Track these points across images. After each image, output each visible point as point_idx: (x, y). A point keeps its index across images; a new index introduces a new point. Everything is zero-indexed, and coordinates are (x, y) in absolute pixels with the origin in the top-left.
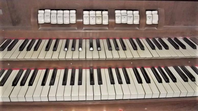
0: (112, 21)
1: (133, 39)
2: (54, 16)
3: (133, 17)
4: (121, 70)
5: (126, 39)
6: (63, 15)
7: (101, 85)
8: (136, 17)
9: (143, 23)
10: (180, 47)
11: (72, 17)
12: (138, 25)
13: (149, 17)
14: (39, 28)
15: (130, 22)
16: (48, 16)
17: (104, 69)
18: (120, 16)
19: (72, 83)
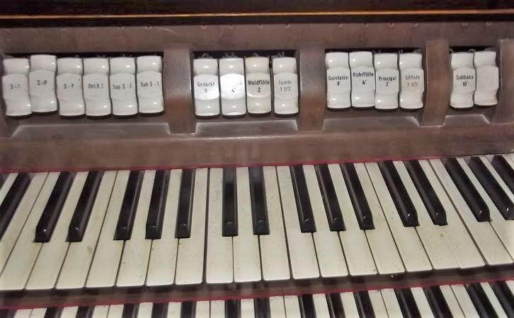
1: (395, 163)
2: (69, 84)
3: (397, 82)
4: (335, 171)
6: (107, 77)
7: (261, 236)
8: (411, 81)
11: (146, 85)
13: (462, 77)
14: (12, 132)
16: (45, 82)
17: (281, 298)
18: (345, 78)
19: (153, 232)
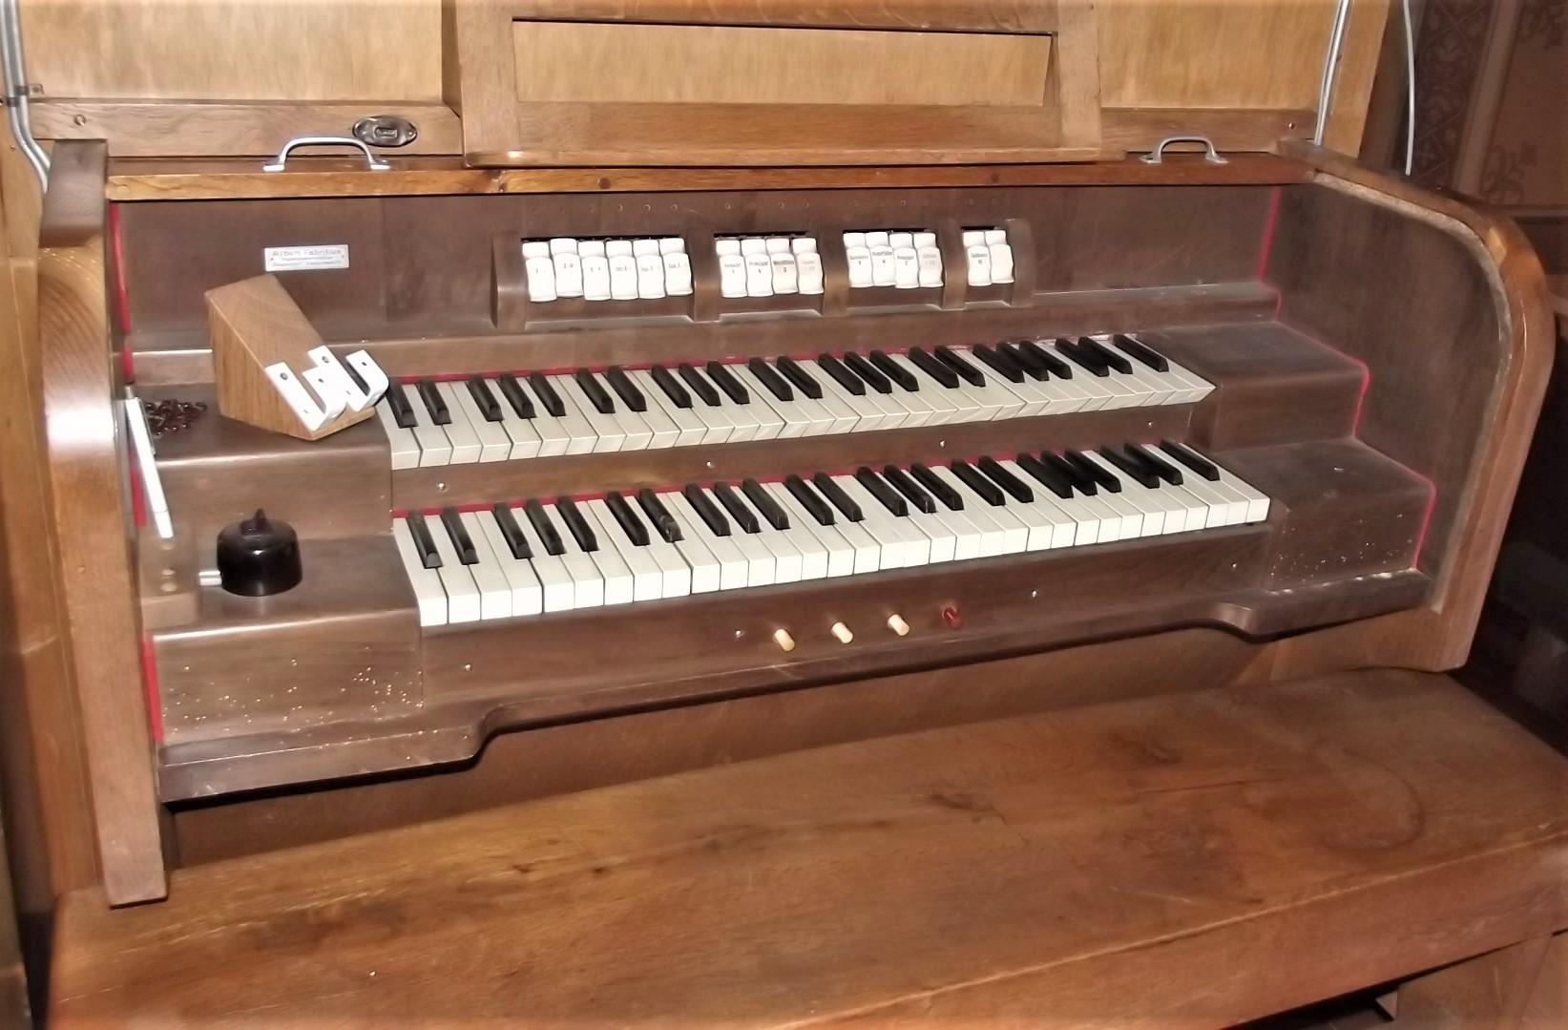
0: (836, 281)
5: (637, 373)
9: (704, 299)
10: (893, 383)
12: (687, 303)
15: (905, 281)
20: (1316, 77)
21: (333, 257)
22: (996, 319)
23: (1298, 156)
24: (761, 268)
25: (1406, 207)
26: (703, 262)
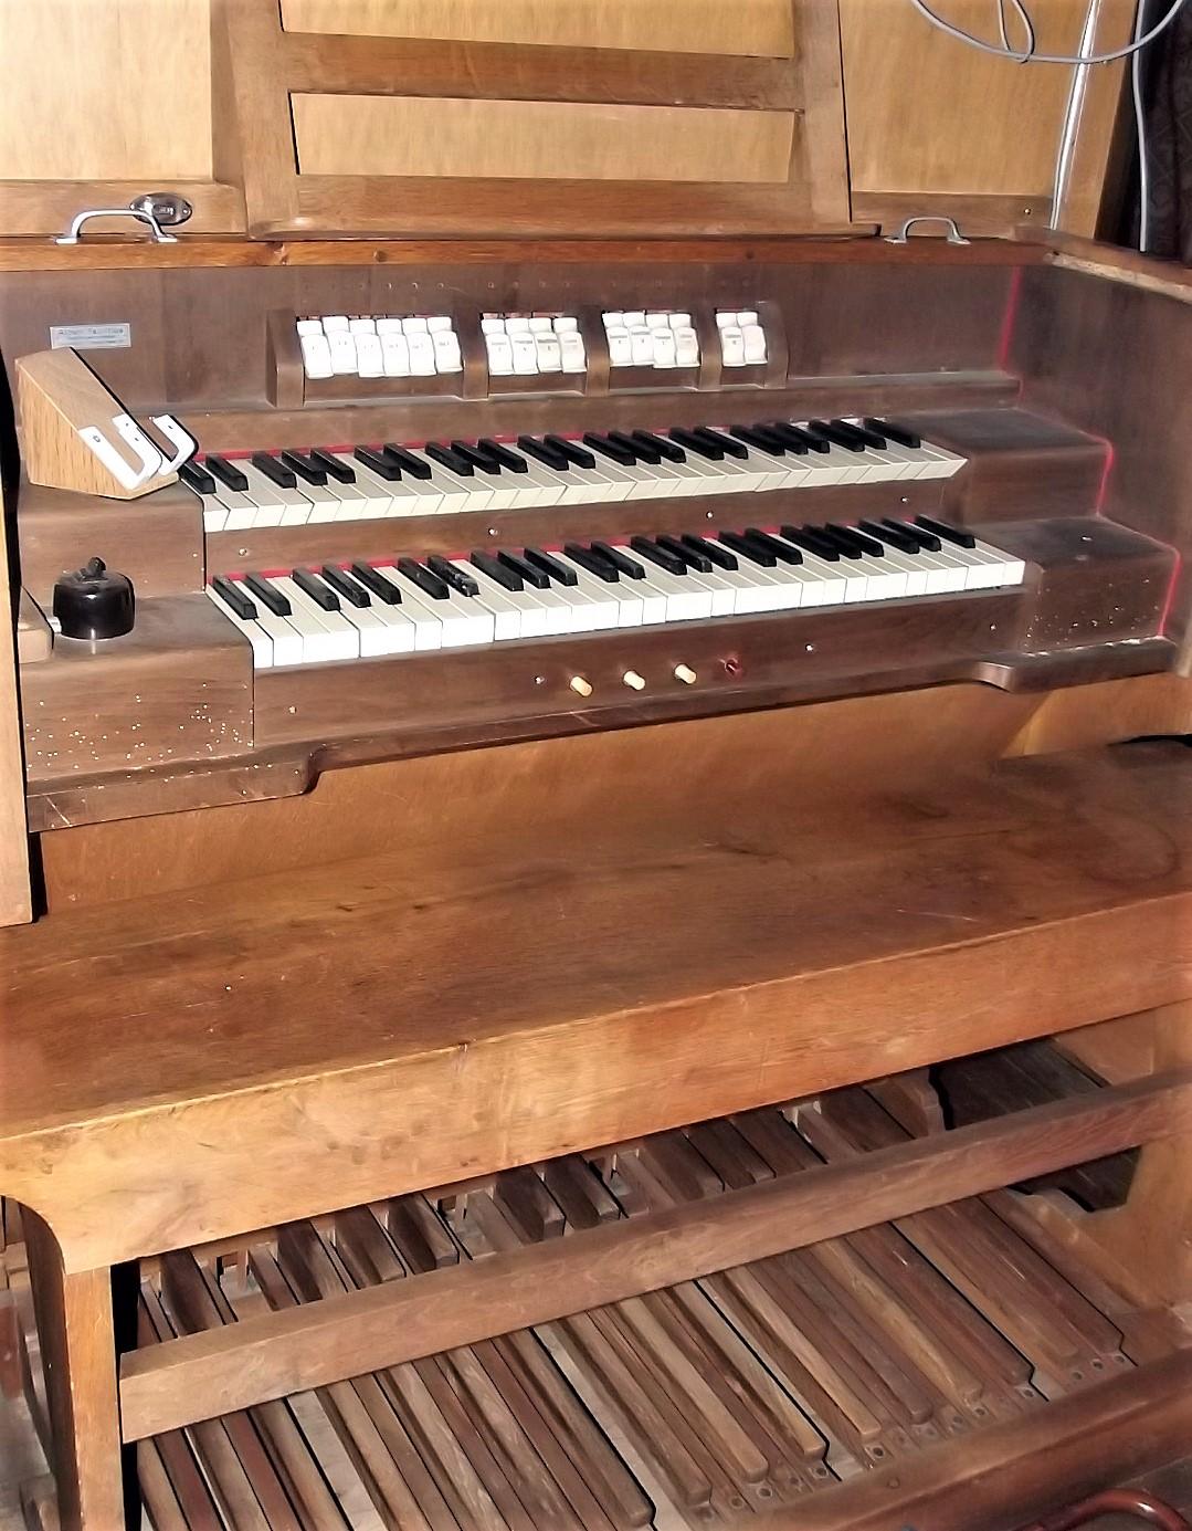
15: (663, 361)
20: (1053, 164)
21: (119, 336)
22: (752, 401)
23: (1036, 241)
24: (528, 345)
25: (1146, 281)
26: (471, 340)
